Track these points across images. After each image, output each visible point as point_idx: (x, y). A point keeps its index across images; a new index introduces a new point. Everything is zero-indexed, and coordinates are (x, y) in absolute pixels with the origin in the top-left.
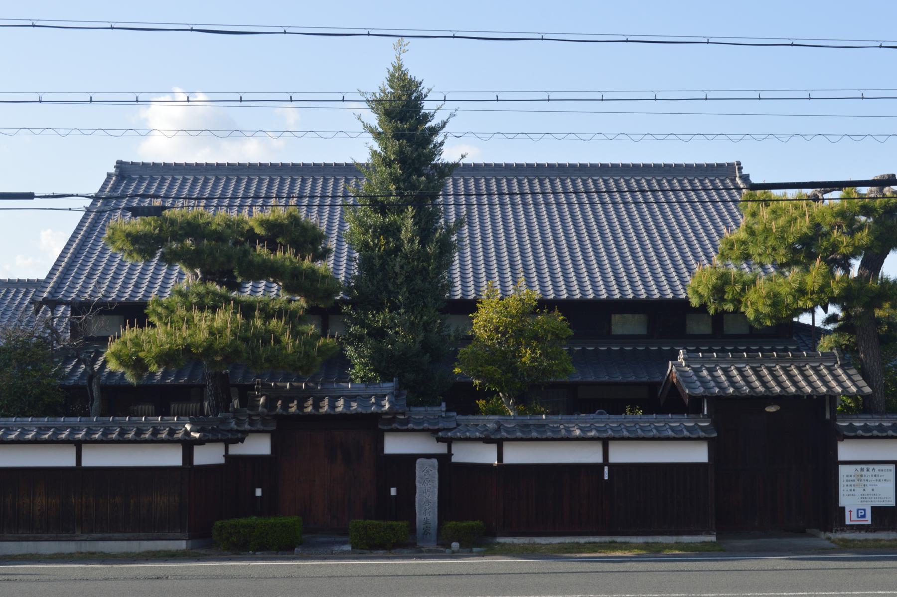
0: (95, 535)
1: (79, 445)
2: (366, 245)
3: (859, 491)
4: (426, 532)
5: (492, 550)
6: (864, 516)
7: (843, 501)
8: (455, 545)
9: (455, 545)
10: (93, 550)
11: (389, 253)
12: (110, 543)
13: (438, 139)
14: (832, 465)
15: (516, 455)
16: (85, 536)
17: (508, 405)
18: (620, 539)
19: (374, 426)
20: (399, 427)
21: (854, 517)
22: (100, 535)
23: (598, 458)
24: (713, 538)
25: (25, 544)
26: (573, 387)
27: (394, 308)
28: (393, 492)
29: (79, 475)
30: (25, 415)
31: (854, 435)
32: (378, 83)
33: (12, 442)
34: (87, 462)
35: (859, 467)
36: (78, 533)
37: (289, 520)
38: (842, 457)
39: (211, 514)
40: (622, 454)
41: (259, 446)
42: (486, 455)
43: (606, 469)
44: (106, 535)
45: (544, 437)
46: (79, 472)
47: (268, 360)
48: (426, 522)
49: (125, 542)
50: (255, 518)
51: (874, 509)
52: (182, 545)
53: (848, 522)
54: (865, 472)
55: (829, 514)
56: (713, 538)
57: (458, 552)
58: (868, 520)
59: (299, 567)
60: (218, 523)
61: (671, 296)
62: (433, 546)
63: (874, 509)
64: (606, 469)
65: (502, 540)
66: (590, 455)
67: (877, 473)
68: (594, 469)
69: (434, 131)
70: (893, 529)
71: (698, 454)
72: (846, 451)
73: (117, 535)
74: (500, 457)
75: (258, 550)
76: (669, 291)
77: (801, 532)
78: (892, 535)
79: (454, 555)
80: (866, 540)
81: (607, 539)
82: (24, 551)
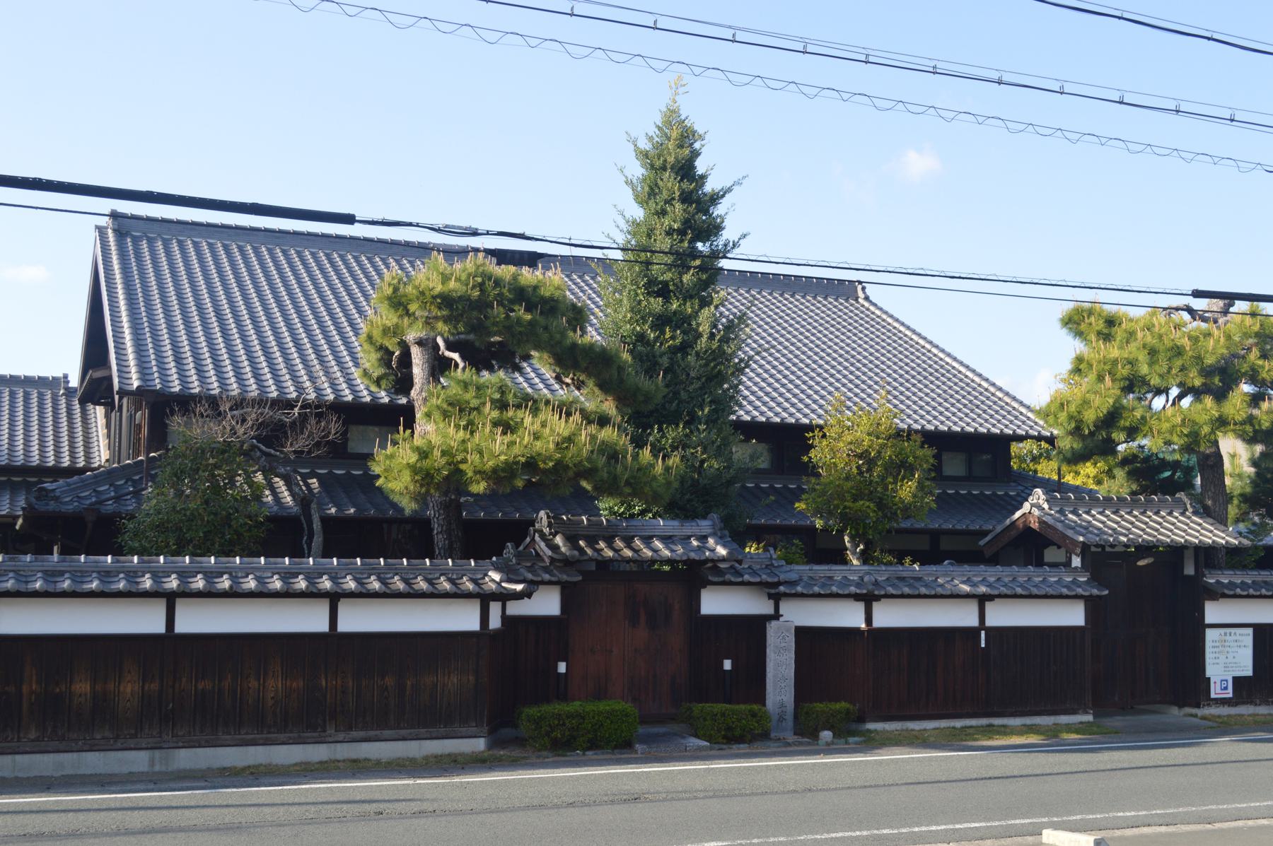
0: (354, 734)
1: (334, 599)
2: (641, 337)
3: (1222, 659)
4: (781, 719)
5: (872, 743)
6: (1226, 688)
7: (1209, 673)
8: (826, 735)
9: (826, 735)
10: (354, 756)
11: (684, 348)
12: (377, 744)
13: (718, 210)
14: (1199, 627)
15: (889, 616)
16: (341, 736)
17: (854, 553)
18: (997, 721)
19: (697, 574)
20: (733, 579)
21: (1218, 690)
22: (362, 734)
23: (971, 620)
24: (1089, 718)
25: (252, 749)
26: (935, 535)
27: (692, 421)
28: (727, 665)
29: (333, 645)
30: (230, 553)
31: (1217, 594)
32: (645, 127)
33: (251, 595)
34: (344, 626)
35: (1222, 631)
36: (330, 731)
37: (619, 705)
38: (1209, 619)
39: (515, 699)
40: (1003, 616)
41: (547, 604)
42: (850, 616)
43: (983, 633)
44: (372, 733)
45: (846, 592)
46: (333, 641)
47: (628, 483)
48: (782, 705)
49: (400, 743)
50: (578, 703)
51: (1235, 679)
52: (479, 744)
53: (1213, 696)
54: (1228, 638)
55: (1187, 683)
56: (1089, 718)
57: (833, 743)
58: (1229, 693)
59: (243, 795)
60: (533, 711)
61: (350, 398)
62: (791, 738)
63: (1235, 679)
64: (983, 633)
65: (871, 726)
66: (962, 616)
67: (1238, 637)
68: (969, 634)
69: (715, 198)
70: (1267, 703)
71: (1072, 615)
72: (1214, 612)
73: (387, 733)
74: (869, 620)
75: (589, 749)
76: (347, 392)
77: (1126, 708)
78: (1263, 710)
79: (829, 750)
80: (1229, 716)
81: (984, 721)
82: (203, 765)
